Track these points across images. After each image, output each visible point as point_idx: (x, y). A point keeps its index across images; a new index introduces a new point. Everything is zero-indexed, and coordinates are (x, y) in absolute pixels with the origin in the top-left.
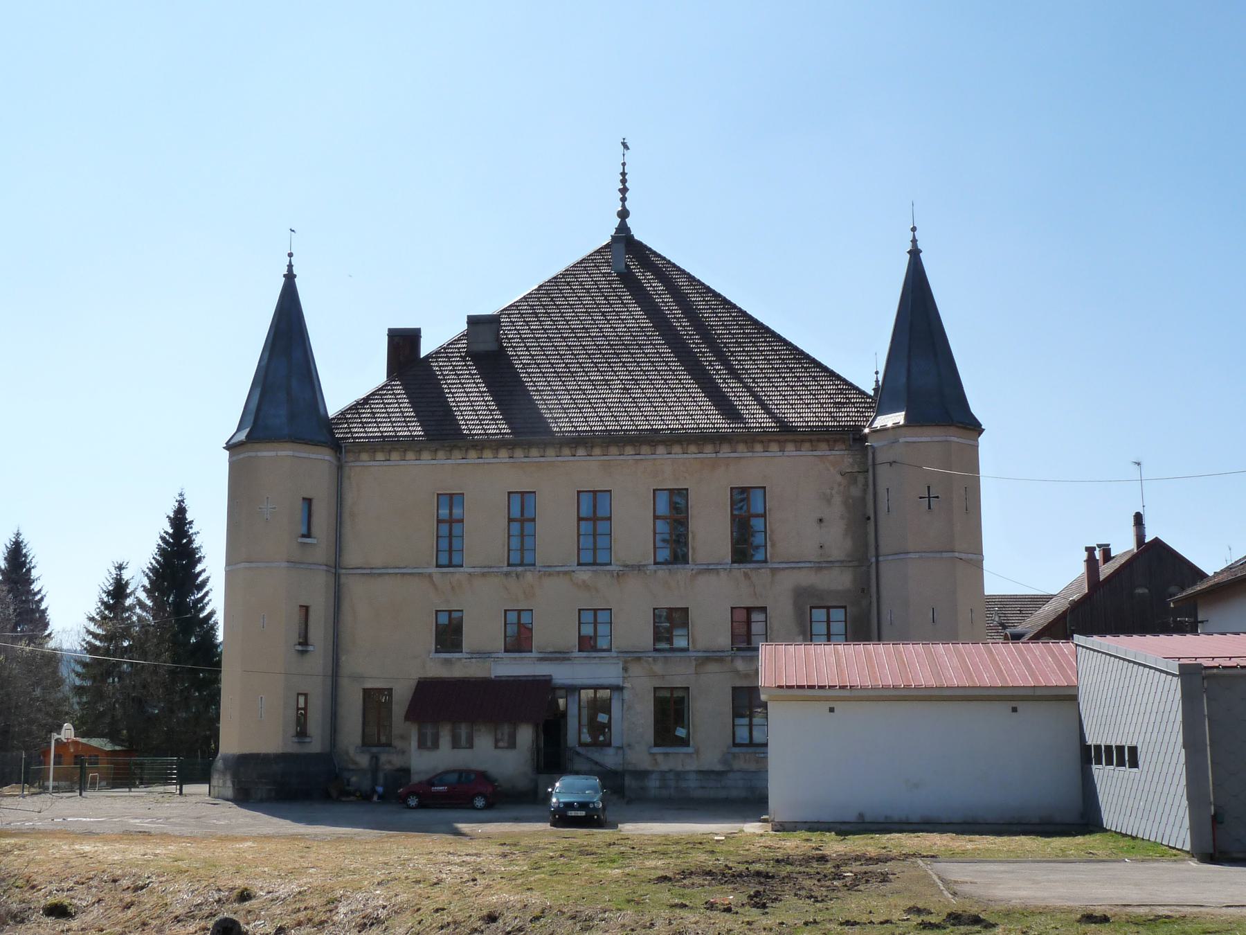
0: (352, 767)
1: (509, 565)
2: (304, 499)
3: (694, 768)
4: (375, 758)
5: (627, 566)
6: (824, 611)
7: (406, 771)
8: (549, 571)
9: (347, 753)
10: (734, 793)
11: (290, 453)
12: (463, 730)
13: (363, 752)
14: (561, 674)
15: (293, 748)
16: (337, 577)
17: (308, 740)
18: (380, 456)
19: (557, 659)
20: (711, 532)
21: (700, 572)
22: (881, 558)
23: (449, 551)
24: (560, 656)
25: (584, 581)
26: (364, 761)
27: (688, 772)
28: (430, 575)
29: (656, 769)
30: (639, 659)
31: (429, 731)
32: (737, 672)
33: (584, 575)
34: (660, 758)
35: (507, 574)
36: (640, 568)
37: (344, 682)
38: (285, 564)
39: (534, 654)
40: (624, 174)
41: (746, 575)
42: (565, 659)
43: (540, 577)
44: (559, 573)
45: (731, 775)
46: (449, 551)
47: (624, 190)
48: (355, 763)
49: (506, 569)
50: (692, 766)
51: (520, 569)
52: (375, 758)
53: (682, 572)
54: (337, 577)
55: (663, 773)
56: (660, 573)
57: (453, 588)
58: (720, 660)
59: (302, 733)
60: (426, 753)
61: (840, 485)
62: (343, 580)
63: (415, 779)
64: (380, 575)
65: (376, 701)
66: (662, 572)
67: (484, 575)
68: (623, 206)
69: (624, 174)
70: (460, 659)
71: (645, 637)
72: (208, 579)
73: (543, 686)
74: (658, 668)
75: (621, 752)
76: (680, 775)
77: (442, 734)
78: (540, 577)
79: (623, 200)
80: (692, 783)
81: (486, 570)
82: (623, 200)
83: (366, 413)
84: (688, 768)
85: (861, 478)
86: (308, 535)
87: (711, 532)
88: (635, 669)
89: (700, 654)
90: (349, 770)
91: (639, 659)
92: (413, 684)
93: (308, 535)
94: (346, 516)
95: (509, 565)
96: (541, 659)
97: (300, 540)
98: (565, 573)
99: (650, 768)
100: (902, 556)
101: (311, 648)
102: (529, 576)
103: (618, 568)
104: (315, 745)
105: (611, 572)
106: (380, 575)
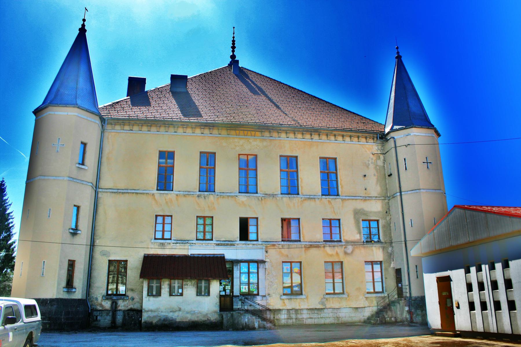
0: (99, 308)
1: (199, 191)
2: (82, 143)
3: (306, 307)
4: (114, 304)
5: (266, 194)
6: (368, 222)
7: (139, 312)
8: (222, 195)
9: (97, 299)
10: (328, 321)
11: (77, 114)
12: (176, 284)
13: (107, 299)
14: (230, 254)
15: (63, 295)
16: (96, 193)
17: (74, 290)
18: (127, 128)
19: (227, 245)
20: (310, 178)
21: (306, 199)
22: (403, 193)
23: (165, 181)
24: (229, 243)
25: (243, 202)
26: (107, 305)
27: (302, 309)
28: (153, 195)
29: (284, 308)
30: (274, 245)
31: (155, 284)
32: (328, 254)
33: (243, 198)
34: (287, 302)
35: (198, 196)
36: (273, 196)
37: (97, 255)
38: (68, 178)
39: (214, 242)
40: (234, 41)
41: (329, 202)
42: (232, 245)
43: (218, 198)
44: (228, 196)
45: (326, 311)
46: (165, 181)
47: (233, 48)
48: (101, 305)
49: (198, 193)
50: (304, 305)
51: (206, 193)
52: (114, 304)
53: (296, 199)
54: (96, 193)
55: (288, 310)
56: (284, 199)
57: (167, 203)
58: (318, 247)
59: (70, 284)
60: (152, 299)
61: (372, 159)
62: (100, 195)
63: (145, 317)
64: (123, 193)
65: (117, 269)
66: (286, 198)
67: (185, 196)
68: (233, 53)
69: (234, 41)
70: (170, 243)
71: (277, 234)
72: (15, 256)
73: (220, 260)
74: (285, 251)
75: (264, 298)
76: (297, 311)
77: (163, 287)
78: (218, 198)
79: (233, 51)
80: (305, 316)
81: (187, 193)
82: (233, 51)
83: (118, 107)
84: (302, 307)
85: (382, 157)
86: (83, 164)
87: (310, 178)
88: (272, 251)
89: (307, 243)
90: (97, 310)
91: (274, 245)
92: (141, 259)
93: (83, 164)
94: (104, 160)
95: (199, 191)
96: (218, 245)
97: (77, 165)
98: (232, 197)
99: (281, 308)
100: (418, 191)
101: (79, 232)
102: (211, 197)
103: (261, 195)
104: (78, 294)
105: (258, 198)
106: (123, 193)
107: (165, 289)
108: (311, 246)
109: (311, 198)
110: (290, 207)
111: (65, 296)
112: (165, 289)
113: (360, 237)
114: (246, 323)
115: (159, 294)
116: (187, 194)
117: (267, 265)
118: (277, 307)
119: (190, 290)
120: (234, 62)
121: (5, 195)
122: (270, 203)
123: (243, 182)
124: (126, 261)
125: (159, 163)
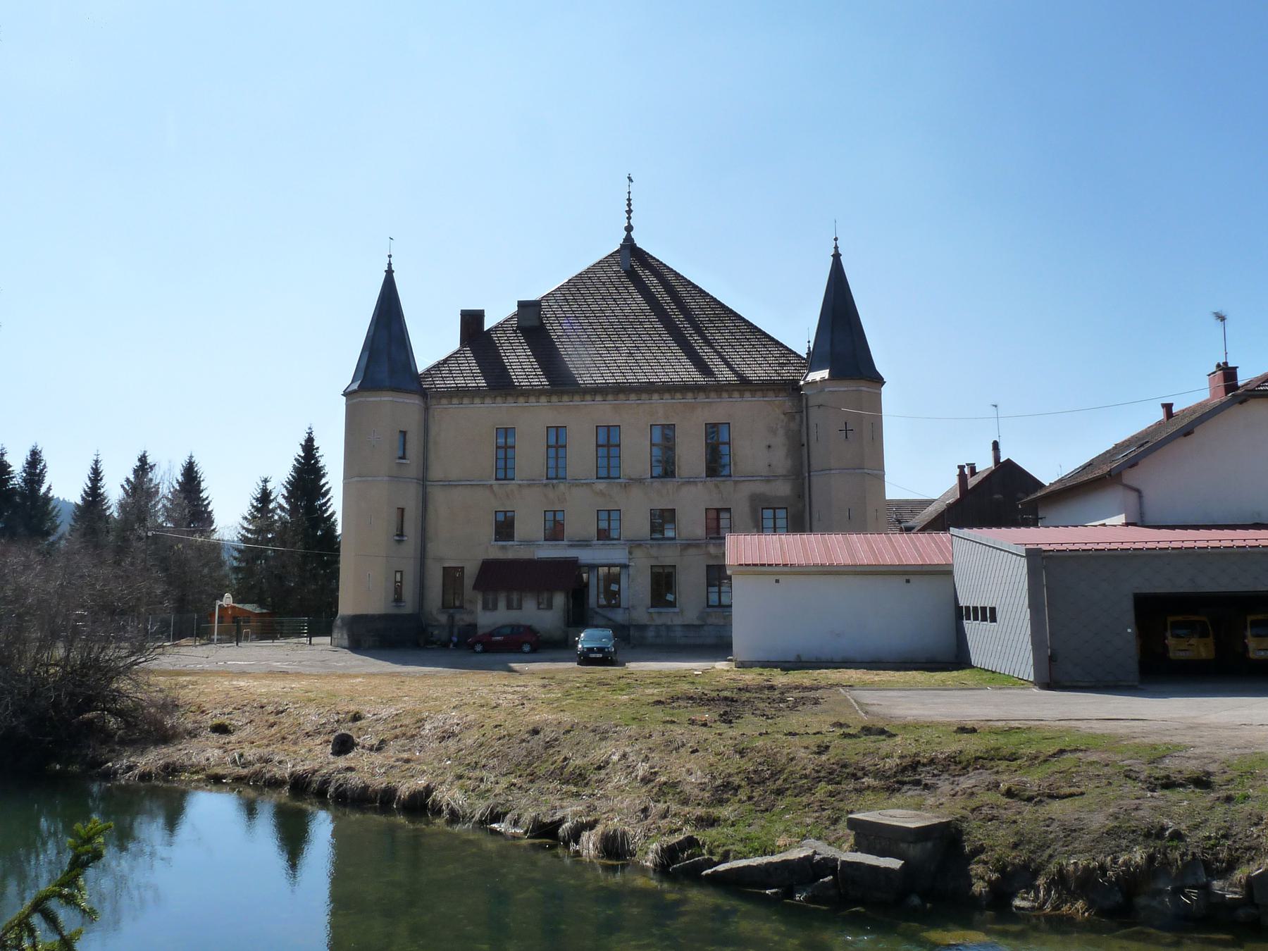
4: (451, 617)
7: (473, 626)
8: (576, 483)
12: (515, 596)
14: (585, 556)
15: (392, 610)
16: (424, 487)
21: (684, 484)
24: (584, 543)
26: (443, 619)
33: (601, 486)
36: (640, 481)
37: (430, 563)
39: (565, 542)
40: (629, 200)
47: (629, 212)
50: (678, 621)
52: (451, 617)
54: (424, 487)
55: (657, 626)
58: (697, 546)
59: (398, 599)
62: (429, 489)
66: (657, 484)
69: (629, 200)
74: (654, 552)
76: (668, 628)
82: (629, 218)
87: (691, 454)
88: (638, 553)
104: (408, 607)
107: (502, 604)
108: (689, 545)
109: (690, 482)
110: (663, 496)
111: (396, 611)
112: (502, 604)
113: (903, 517)
114: (85, 535)
115: (495, 608)
116: (532, 483)
117: (631, 571)
118: (642, 622)
119: (530, 605)
120: (629, 241)
121: (324, 475)
122: (636, 492)
123: (614, 462)
124: (462, 568)
125: (220, 641)
